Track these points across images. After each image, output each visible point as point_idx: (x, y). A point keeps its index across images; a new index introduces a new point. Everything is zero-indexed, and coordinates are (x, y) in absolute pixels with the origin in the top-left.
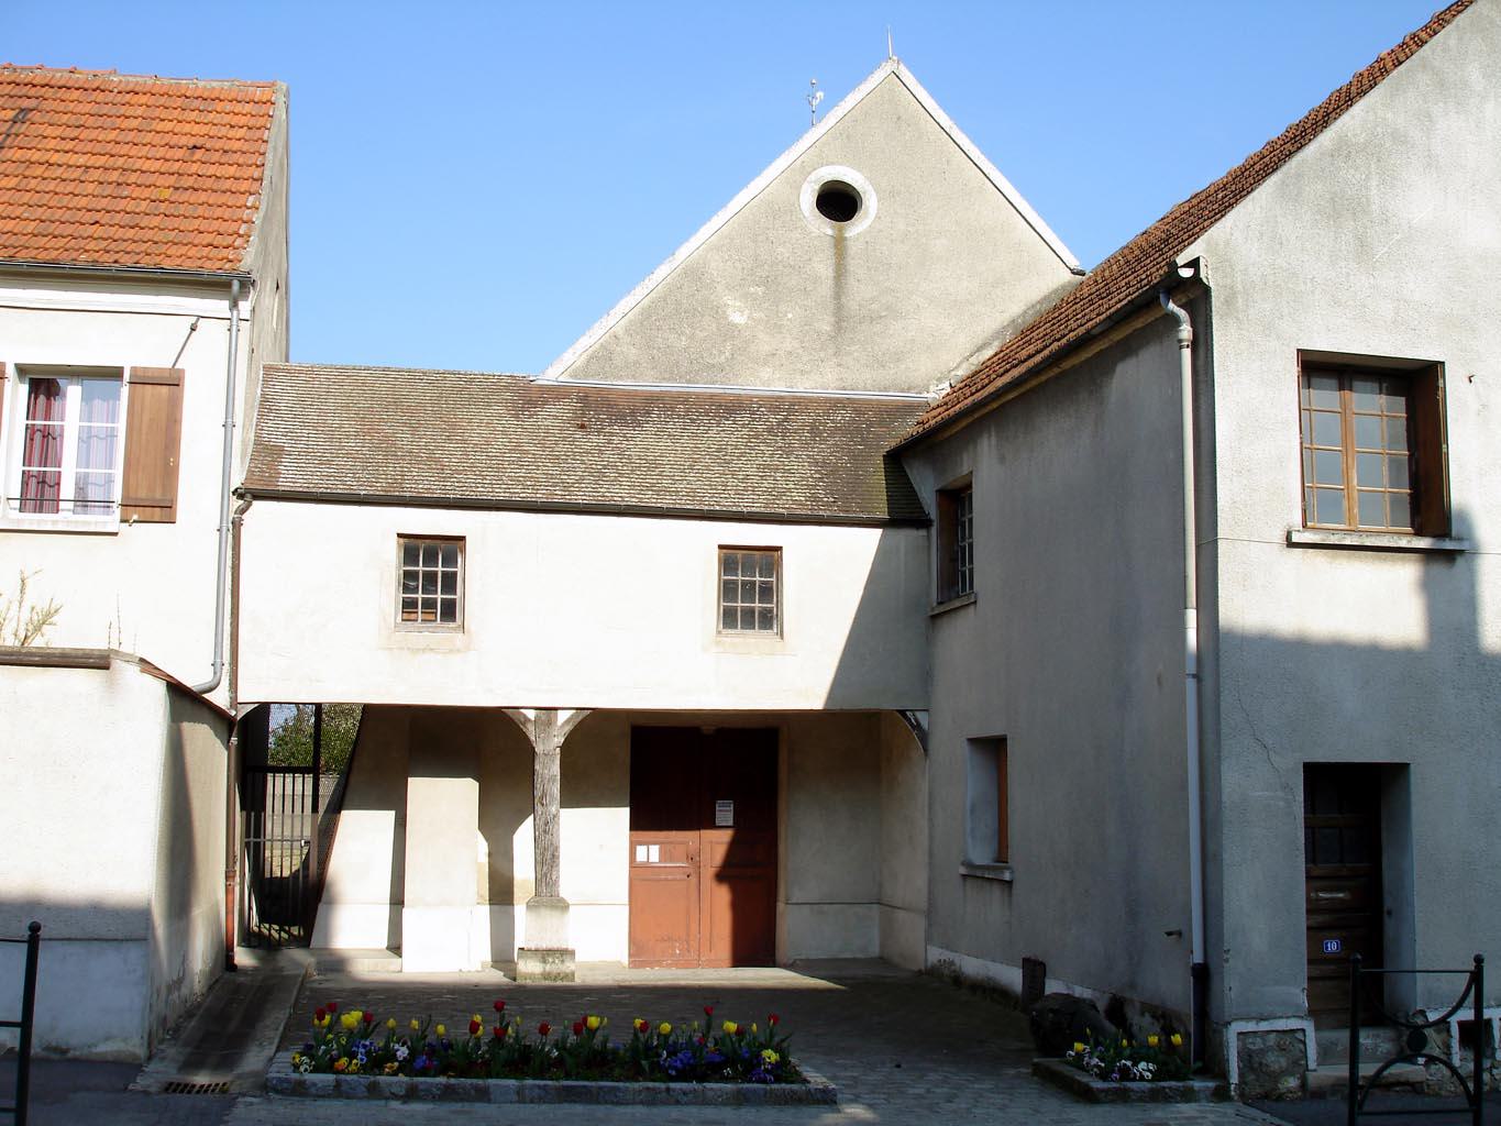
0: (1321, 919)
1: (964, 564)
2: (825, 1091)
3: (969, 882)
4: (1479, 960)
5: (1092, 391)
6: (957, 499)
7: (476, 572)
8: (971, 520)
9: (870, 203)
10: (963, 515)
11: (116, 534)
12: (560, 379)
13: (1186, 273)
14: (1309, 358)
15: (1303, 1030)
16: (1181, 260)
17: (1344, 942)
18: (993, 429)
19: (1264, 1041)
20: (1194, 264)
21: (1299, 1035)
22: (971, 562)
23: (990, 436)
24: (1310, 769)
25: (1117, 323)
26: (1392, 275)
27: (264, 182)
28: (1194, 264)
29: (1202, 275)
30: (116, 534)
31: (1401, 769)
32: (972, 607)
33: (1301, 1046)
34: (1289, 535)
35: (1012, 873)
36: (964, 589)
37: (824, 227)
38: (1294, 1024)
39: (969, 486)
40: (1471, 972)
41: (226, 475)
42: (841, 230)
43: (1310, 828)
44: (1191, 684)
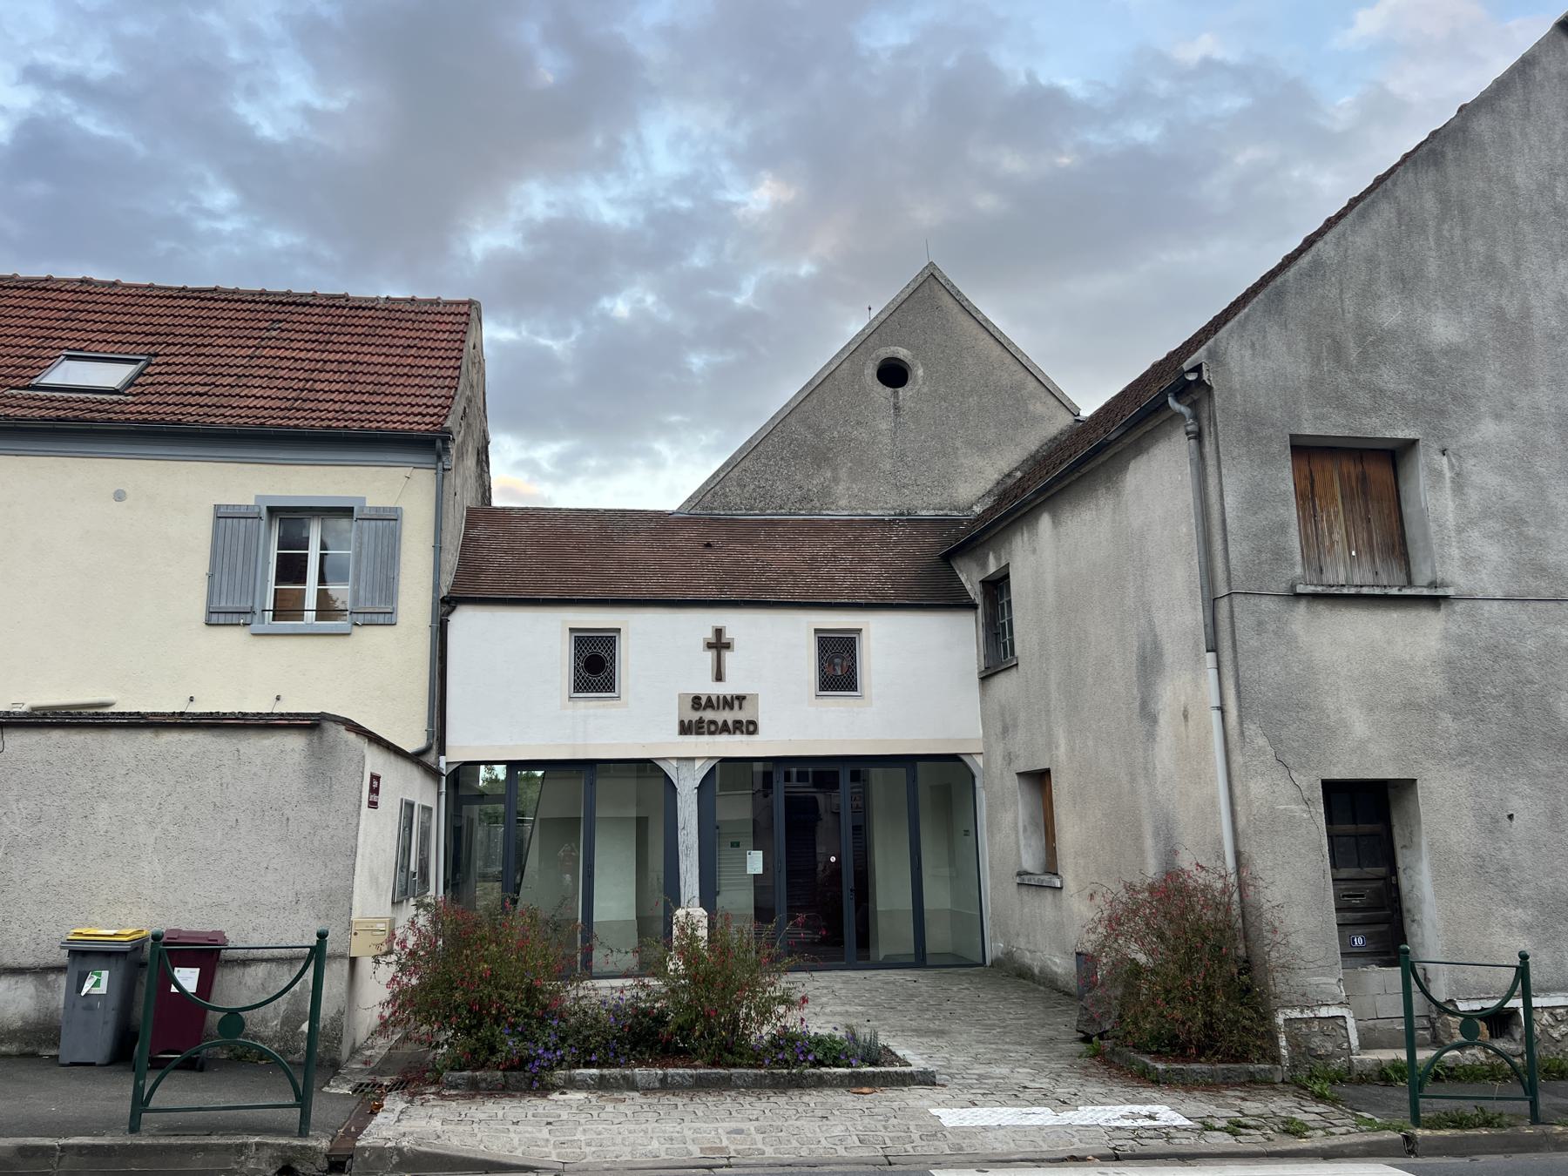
0: (1350, 916)
1: (1004, 637)
2: (925, 1073)
3: (1024, 889)
4: (1524, 957)
5: (1109, 488)
6: (997, 587)
7: (630, 661)
8: (1009, 602)
9: (919, 372)
10: (1002, 598)
11: (349, 634)
12: (692, 512)
13: (1192, 377)
14: (1298, 442)
15: (1343, 1017)
16: (1186, 366)
17: (1367, 938)
18: (1026, 535)
19: (1309, 1028)
20: (1197, 369)
21: (1340, 1022)
22: (1011, 633)
23: (1022, 534)
24: (1332, 789)
25: (1131, 428)
26: (1368, 370)
27: (463, 369)
28: (1197, 369)
29: (1205, 377)
30: (349, 634)
31: (1408, 785)
32: (1015, 669)
33: (1343, 1031)
34: (1293, 587)
35: (1062, 882)
36: (1006, 656)
37: (882, 392)
38: (1335, 1011)
39: (1007, 576)
40: (1517, 968)
41: (436, 587)
42: (896, 395)
43: (1331, 837)
44: (1216, 715)
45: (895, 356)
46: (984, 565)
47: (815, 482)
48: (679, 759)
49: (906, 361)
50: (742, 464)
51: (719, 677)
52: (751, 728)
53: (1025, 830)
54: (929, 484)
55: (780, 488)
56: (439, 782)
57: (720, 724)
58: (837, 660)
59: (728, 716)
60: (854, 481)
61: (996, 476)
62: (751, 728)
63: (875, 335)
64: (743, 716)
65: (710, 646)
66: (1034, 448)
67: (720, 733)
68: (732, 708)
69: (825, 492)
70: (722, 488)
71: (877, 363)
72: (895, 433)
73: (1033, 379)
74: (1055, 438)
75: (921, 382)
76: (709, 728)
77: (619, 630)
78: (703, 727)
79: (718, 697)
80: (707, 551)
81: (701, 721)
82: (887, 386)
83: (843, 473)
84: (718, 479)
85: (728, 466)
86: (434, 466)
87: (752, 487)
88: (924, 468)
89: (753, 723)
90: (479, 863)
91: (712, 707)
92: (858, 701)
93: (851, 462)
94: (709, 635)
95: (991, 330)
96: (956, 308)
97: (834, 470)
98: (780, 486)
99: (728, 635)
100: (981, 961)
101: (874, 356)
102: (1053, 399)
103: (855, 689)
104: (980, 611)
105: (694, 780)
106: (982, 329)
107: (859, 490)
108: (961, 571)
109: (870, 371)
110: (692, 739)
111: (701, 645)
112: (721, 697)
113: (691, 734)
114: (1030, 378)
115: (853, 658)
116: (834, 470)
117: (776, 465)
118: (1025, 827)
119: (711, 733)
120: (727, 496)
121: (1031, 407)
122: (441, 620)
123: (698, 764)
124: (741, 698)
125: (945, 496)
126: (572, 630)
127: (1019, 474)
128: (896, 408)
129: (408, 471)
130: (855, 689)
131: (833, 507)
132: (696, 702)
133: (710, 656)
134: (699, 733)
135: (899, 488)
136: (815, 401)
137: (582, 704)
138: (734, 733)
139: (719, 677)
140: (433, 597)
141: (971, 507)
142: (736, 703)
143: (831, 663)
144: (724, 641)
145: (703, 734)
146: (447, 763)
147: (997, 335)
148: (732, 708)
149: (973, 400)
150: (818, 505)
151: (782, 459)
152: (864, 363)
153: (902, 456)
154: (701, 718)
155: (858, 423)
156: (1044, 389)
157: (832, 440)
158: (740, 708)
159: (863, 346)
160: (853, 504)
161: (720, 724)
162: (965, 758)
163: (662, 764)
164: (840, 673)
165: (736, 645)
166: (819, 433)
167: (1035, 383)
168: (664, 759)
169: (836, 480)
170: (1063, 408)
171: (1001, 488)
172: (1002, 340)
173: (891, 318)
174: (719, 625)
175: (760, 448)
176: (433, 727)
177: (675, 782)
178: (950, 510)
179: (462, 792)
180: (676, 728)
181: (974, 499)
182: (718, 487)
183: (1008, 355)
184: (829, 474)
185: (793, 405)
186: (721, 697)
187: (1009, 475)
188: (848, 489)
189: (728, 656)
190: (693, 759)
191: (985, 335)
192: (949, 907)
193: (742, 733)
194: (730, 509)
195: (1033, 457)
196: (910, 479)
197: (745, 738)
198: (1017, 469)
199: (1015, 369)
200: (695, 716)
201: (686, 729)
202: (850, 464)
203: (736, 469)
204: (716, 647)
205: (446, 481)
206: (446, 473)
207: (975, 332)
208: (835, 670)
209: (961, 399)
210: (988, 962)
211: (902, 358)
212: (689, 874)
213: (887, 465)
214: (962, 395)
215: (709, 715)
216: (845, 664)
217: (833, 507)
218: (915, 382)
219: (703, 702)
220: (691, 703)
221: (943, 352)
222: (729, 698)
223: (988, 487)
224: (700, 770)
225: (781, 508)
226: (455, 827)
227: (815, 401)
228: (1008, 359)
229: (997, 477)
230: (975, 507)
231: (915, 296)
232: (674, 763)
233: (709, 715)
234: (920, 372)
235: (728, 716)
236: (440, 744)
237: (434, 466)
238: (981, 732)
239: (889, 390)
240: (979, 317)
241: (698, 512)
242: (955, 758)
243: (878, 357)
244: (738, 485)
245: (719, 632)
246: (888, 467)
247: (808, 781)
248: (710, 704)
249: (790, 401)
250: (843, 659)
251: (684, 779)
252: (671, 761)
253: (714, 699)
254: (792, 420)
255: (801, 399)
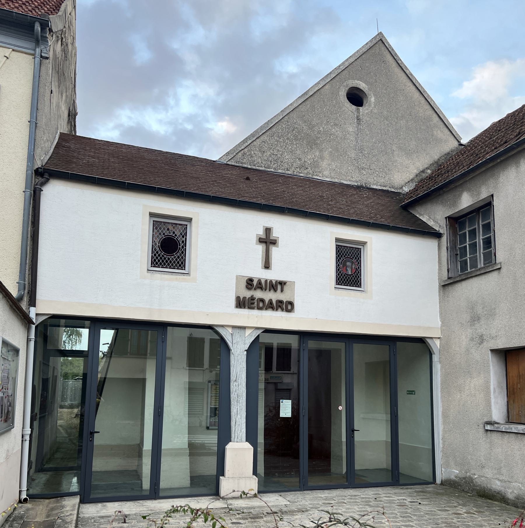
41: (31, 157)
45: (357, 86)
46: (479, 194)
47: (309, 157)
48: (234, 327)
49: (365, 91)
50: (262, 138)
51: (267, 266)
52: (289, 307)
53: (494, 392)
54: (378, 170)
55: (287, 157)
56: (29, 330)
57: (267, 302)
58: (348, 264)
59: (269, 296)
60: (333, 160)
61: (415, 171)
62: (289, 307)
63: (346, 72)
64: (284, 297)
65: (261, 241)
66: (436, 157)
67: (266, 309)
68: (275, 290)
69: (315, 165)
70: (249, 151)
71: (347, 89)
72: (357, 135)
73: (436, 116)
74: (449, 153)
75: (373, 106)
76: (258, 305)
77: (190, 220)
78: (253, 303)
79: (266, 281)
80: (247, 182)
81: (252, 298)
82: (353, 104)
83: (326, 154)
84: (247, 144)
85: (253, 137)
86: (32, 52)
87: (269, 153)
88: (374, 159)
89: (291, 303)
90: (59, 399)
91: (261, 288)
92: (363, 294)
93: (331, 148)
94: (261, 232)
95: (414, 81)
96: (394, 64)
97: (321, 151)
98: (287, 157)
99: (275, 234)
100: (431, 480)
101: (345, 84)
102: (447, 130)
103: (360, 286)
104: (444, 239)
105: (245, 344)
106: (409, 80)
107: (336, 167)
108: (421, 215)
109: (343, 94)
110: (245, 312)
111: (254, 240)
112: (268, 282)
113: (245, 308)
114: (435, 115)
115: (359, 263)
116: (321, 151)
117: (284, 142)
118: (494, 389)
119: (259, 308)
120: (252, 157)
121: (435, 132)
122: (35, 188)
123: (248, 332)
124: (282, 284)
125: (387, 178)
126: (152, 215)
127: (429, 171)
128: (358, 119)
129: (8, 52)
130: (360, 286)
131: (320, 175)
132: (250, 283)
133: (260, 249)
134: (251, 308)
135: (360, 169)
136: (308, 106)
137: (158, 276)
138: (277, 310)
139: (267, 266)
140: (28, 166)
141: (402, 188)
142: (279, 287)
143: (345, 265)
144: (271, 238)
145: (253, 308)
146: (37, 315)
147: (418, 86)
148: (275, 290)
149: (403, 123)
150: (311, 172)
151: (288, 139)
152: (339, 88)
153: (361, 150)
154: (252, 296)
155: (336, 125)
156: (442, 123)
157: (319, 132)
158: (282, 291)
159: (338, 76)
160: (332, 174)
161: (267, 302)
162: (429, 341)
163: (220, 330)
164: (350, 273)
165: (280, 242)
166: (311, 127)
167: (437, 119)
168: (222, 326)
169: (322, 158)
170: (452, 136)
171: (419, 178)
172: (420, 88)
173: (356, 62)
174: (268, 225)
175: (274, 130)
176: (24, 281)
177: (230, 344)
178: (390, 187)
179: (50, 347)
180: (233, 302)
181: (403, 183)
182: (246, 150)
183: (423, 99)
184: (317, 154)
185: (295, 105)
186: (268, 282)
187: (423, 171)
188: (329, 165)
189: (274, 251)
190: (244, 328)
191: (410, 84)
192: (385, 439)
193: (282, 310)
194: (254, 166)
195: (436, 162)
196: (366, 165)
197: (284, 314)
198: (427, 168)
199: (426, 108)
200: (248, 294)
201: (241, 303)
202: (330, 149)
203: (258, 140)
204: (266, 242)
205: (43, 68)
206: (45, 61)
207: (404, 81)
208: (347, 270)
209: (396, 121)
210: (438, 481)
211: (362, 88)
212: (239, 416)
213: (352, 154)
214: (397, 119)
215: (258, 294)
216: (354, 267)
217: (320, 175)
218: (370, 105)
219: (255, 283)
220: (245, 284)
221: (386, 89)
222: (274, 282)
223: (411, 177)
224: (249, 337)
225: (288, 170)
226: (43, 379)
227: (308, 106)
228: (423, 101)
229: (416, 171)
230: (404, 188)
231: (370, 51)
232: (230, 330)
233: (258, 294)
234: (373, 99)
235: (269, 296)
236: (30, 297)
237: (32, 52)
238: (440, 323)
239: (354, 107)
240: (407, 72)
241: (233, 164)
242: (421, 341)
243: (347, 85)
244: (260, 150)
245: (268, 231)
246: (353, 155)
247: (338, 351)
248: (260, 286)
249: (294, 102)
250: (352, 263)
251: (237, 343)
252: (228, 328)
253: (263, 282)
254: (294, 115)
255: (300, 102)
